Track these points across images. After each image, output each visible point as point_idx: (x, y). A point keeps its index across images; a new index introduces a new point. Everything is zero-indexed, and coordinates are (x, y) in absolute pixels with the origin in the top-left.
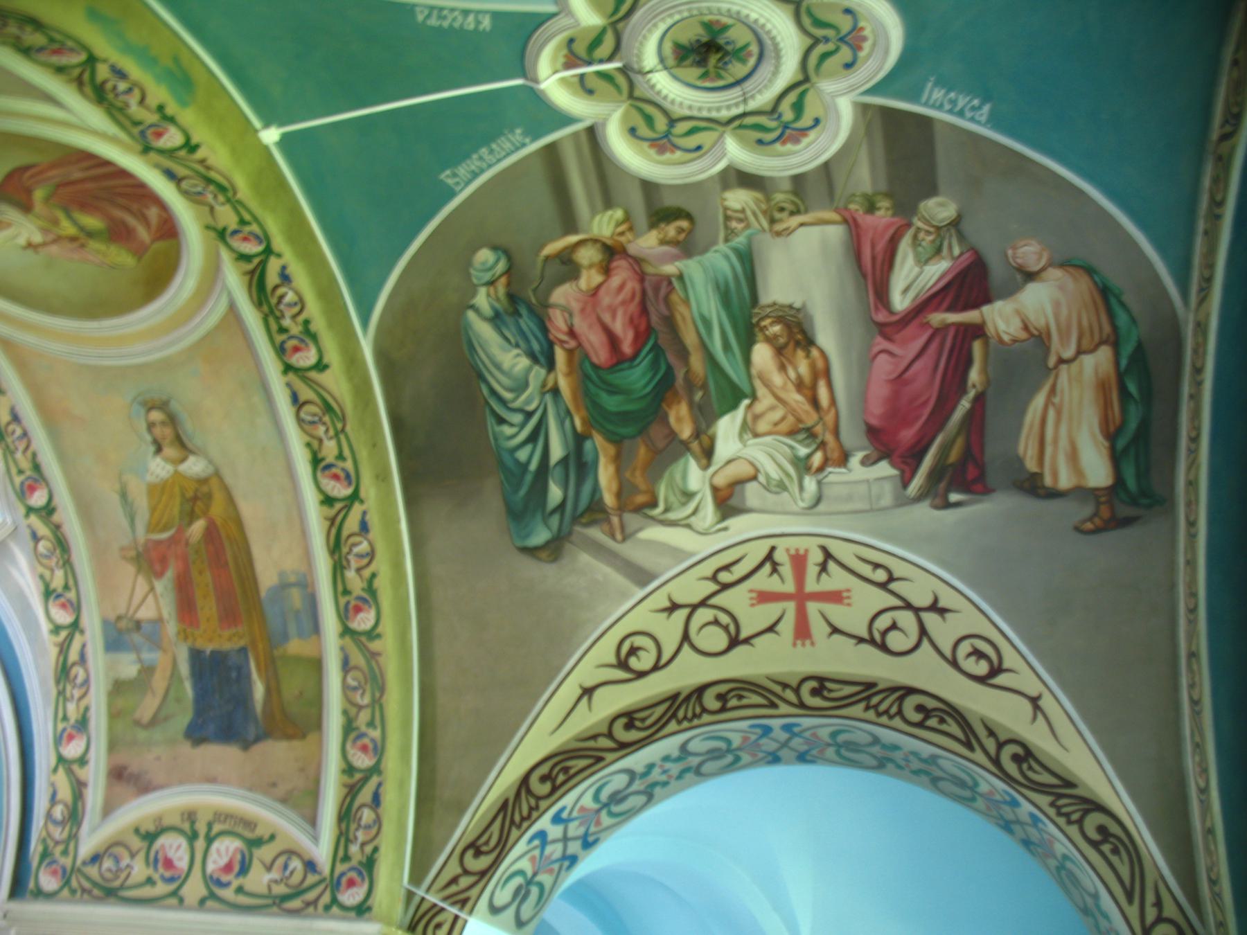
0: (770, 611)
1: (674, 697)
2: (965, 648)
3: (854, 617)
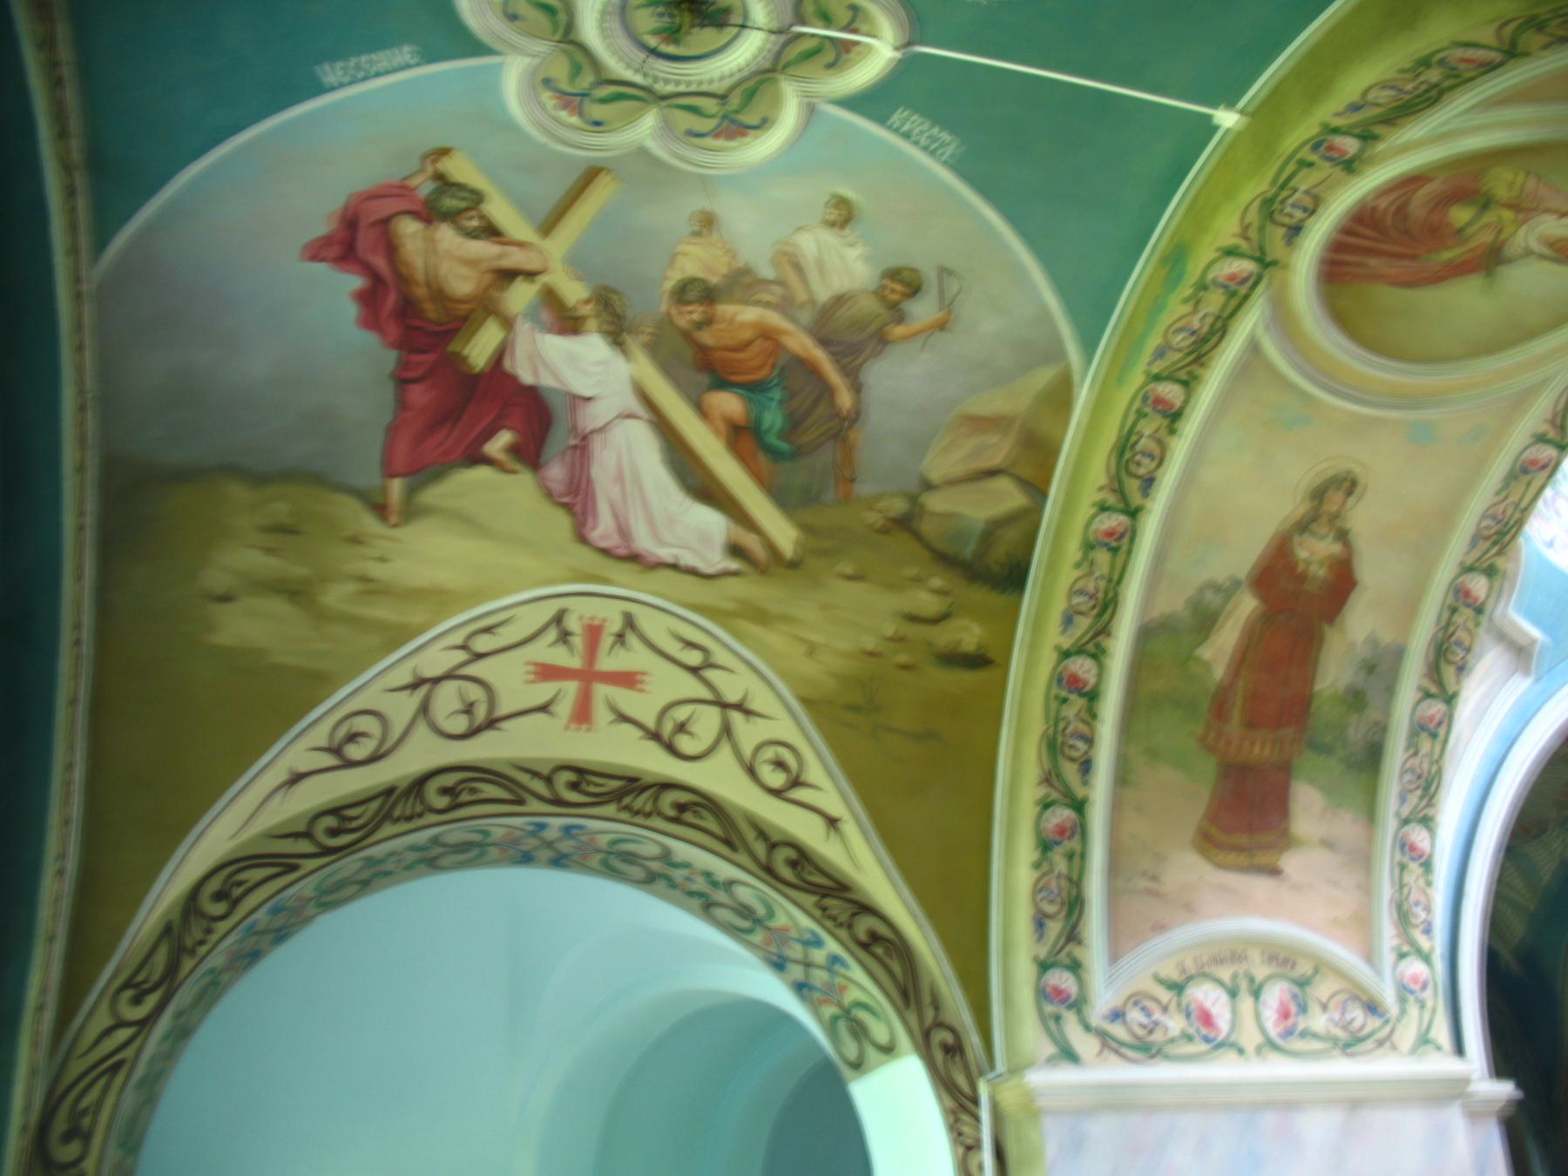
0: (544, 691)
1: (389, 792)
2: (770, 753)
3: (644, 706)
